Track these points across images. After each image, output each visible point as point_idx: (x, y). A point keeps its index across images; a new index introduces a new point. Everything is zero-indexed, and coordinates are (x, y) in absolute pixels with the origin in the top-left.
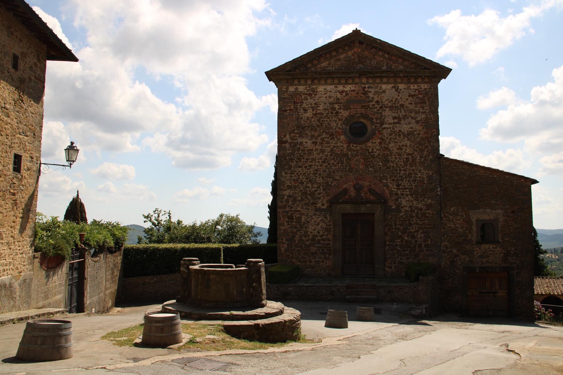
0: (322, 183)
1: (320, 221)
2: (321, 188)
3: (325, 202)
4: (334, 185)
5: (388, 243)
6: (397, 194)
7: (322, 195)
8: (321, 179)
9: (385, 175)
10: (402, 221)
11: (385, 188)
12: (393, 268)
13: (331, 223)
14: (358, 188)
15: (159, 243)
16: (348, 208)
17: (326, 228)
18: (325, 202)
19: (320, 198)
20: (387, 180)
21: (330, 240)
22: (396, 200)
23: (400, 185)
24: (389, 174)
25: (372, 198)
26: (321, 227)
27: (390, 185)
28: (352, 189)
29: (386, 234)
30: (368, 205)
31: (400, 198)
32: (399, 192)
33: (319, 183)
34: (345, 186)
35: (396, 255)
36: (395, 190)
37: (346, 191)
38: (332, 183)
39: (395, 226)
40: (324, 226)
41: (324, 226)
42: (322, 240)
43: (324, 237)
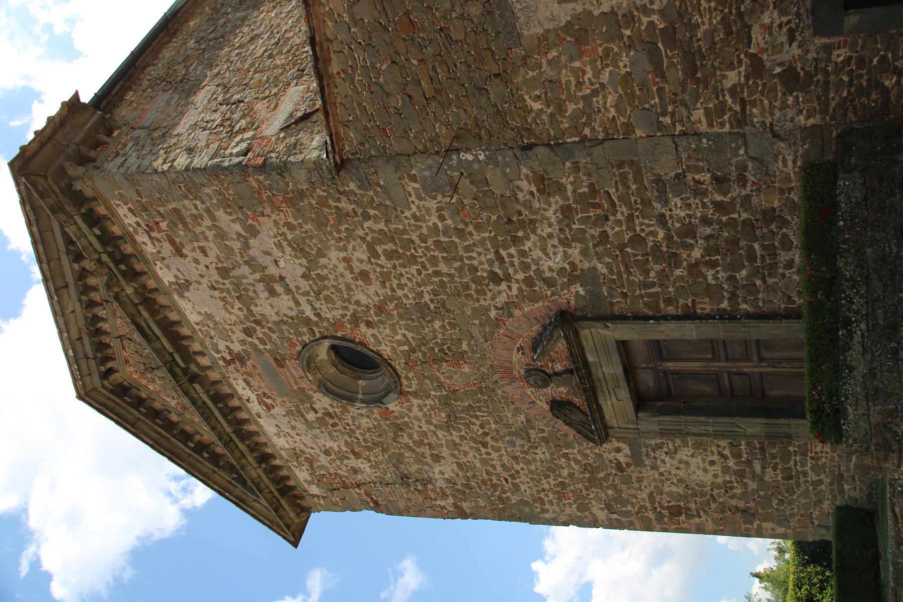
6: (529, 281)
10: (627, 268)
26: (692, 456)
30: (590, 359)
32: (521, 276)
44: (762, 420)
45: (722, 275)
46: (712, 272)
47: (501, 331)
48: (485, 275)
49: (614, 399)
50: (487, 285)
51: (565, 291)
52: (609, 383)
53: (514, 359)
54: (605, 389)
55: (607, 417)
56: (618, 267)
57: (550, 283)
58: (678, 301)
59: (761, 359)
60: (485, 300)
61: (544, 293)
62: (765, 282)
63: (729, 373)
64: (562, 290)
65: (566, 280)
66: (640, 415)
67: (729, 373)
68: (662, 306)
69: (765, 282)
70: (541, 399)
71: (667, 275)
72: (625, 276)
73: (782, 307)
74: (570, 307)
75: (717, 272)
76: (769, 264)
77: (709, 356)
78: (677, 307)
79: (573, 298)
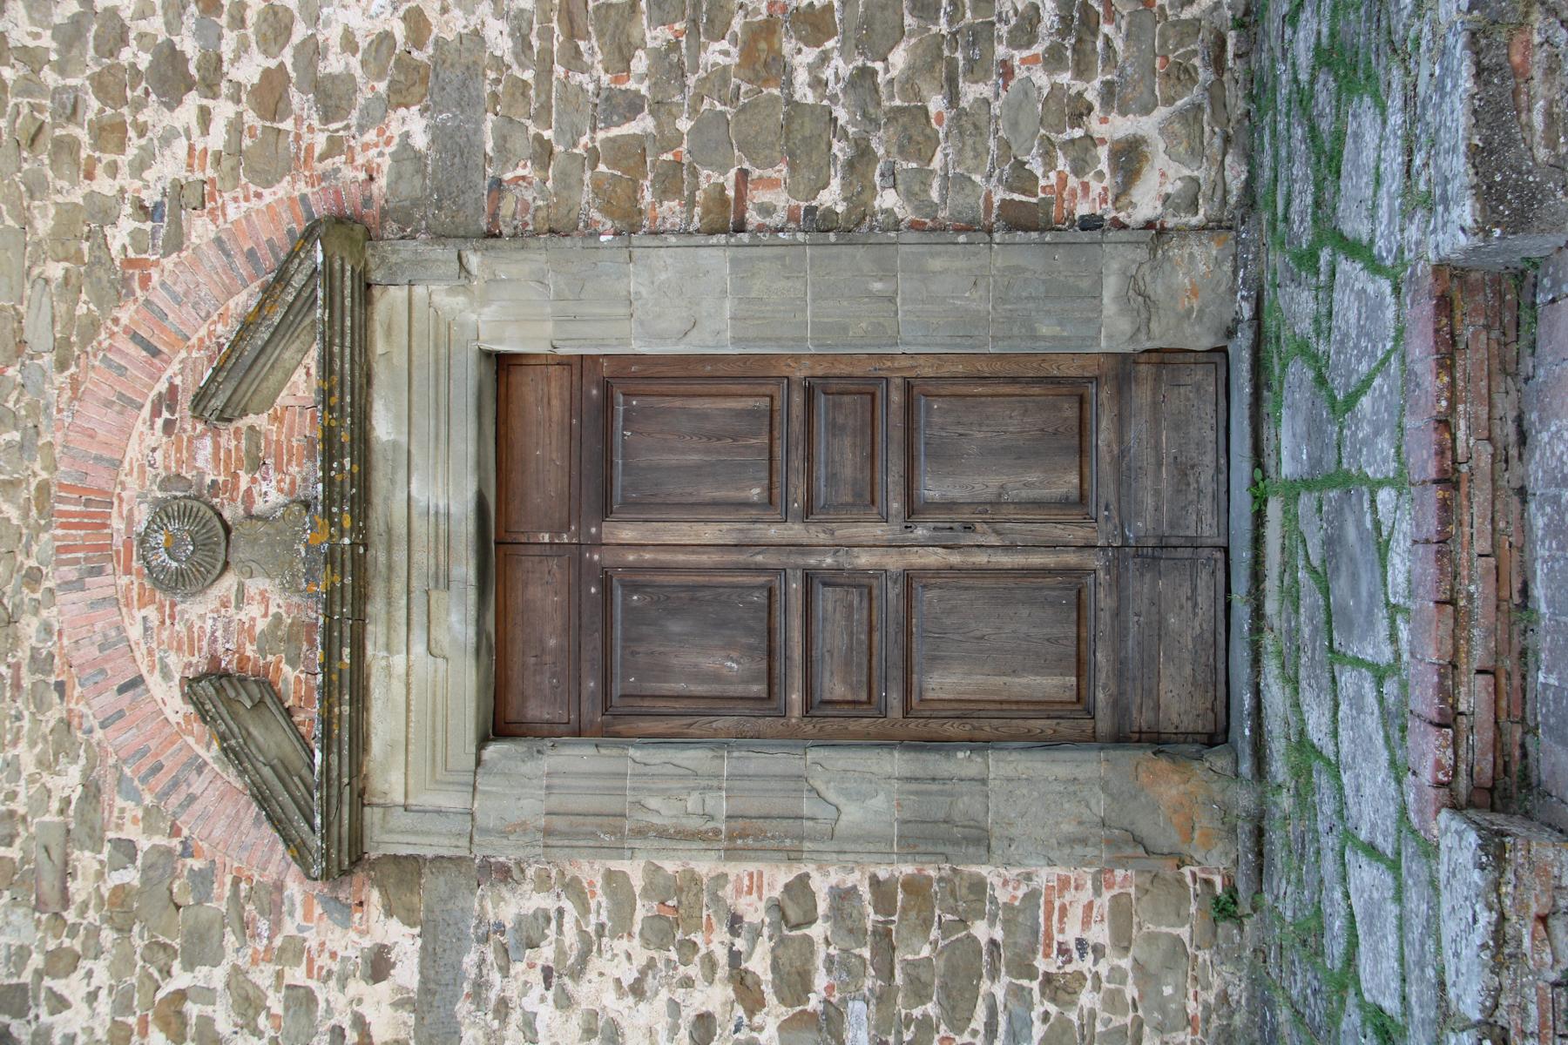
0: (123, 963)
1: (565, 1002)
2: (181, 979)
3: (348, 943)
4: (150, 818)
5: (832, 197)
6: (270, 96)
7: (263, 977)
8: (72, 987)
9: (44, 225)
10: (572, 34)
11: (200, 229)
12: (1146, 125)
13: (590, 871)
14: (199, 538)
15: (25, 964)
16: (423, 666)
17: (660, 933)
18: (348, 943)
19: (301, 1000)
20: (104, 213)
21: (800, 888)
22: (332, 98)
23: (170, 57)
24: (36, 187)
25: (300, 383)
26: (637, 990)
27: (170, 167)
28: (200, 611)
29: (727, 221)
30: (384, 428)
31: (312, 51)
32: (248, 70)
33: (123, 1004)
34: (175, 707)
35: (971, 92)
36: (223, 110)
37: (221, 690)
38: (127, 849)
39: (633, 106)
40: (623, 958)
41: (623, 958)
42: (794, 983)
43: (759, 964)
44: (895, 763)
45: (840, 67)
46: (810, 55)
47: (126, 315)
48: (144, 61)
49: (419, 648)
50: (139, 106)
51: (371, 136)
52: (419, 556)
53: (133, 452)
54: (399, 586)
55: (377, 746)
56: (546, 34)
57: (332, 98)
58: (695, 174)
59: (913, 509)
60: (113, 170)
61: (307, 138)
62: (953, 98)
63: (809, 577)
64: (362, 129)
65: (382, 87)
66: (493, 750)
67: (809, 577)
68: (648, 196)
69: (953, 98)
70: (166, 641)
71: (680, 64)
72: (559, 70)
73: (996, 200)
74: (368, 201)
75: (824, 58)
76: (970, 27)
77: (755, 493)
78: (691, 203)
79: (386, 163)
